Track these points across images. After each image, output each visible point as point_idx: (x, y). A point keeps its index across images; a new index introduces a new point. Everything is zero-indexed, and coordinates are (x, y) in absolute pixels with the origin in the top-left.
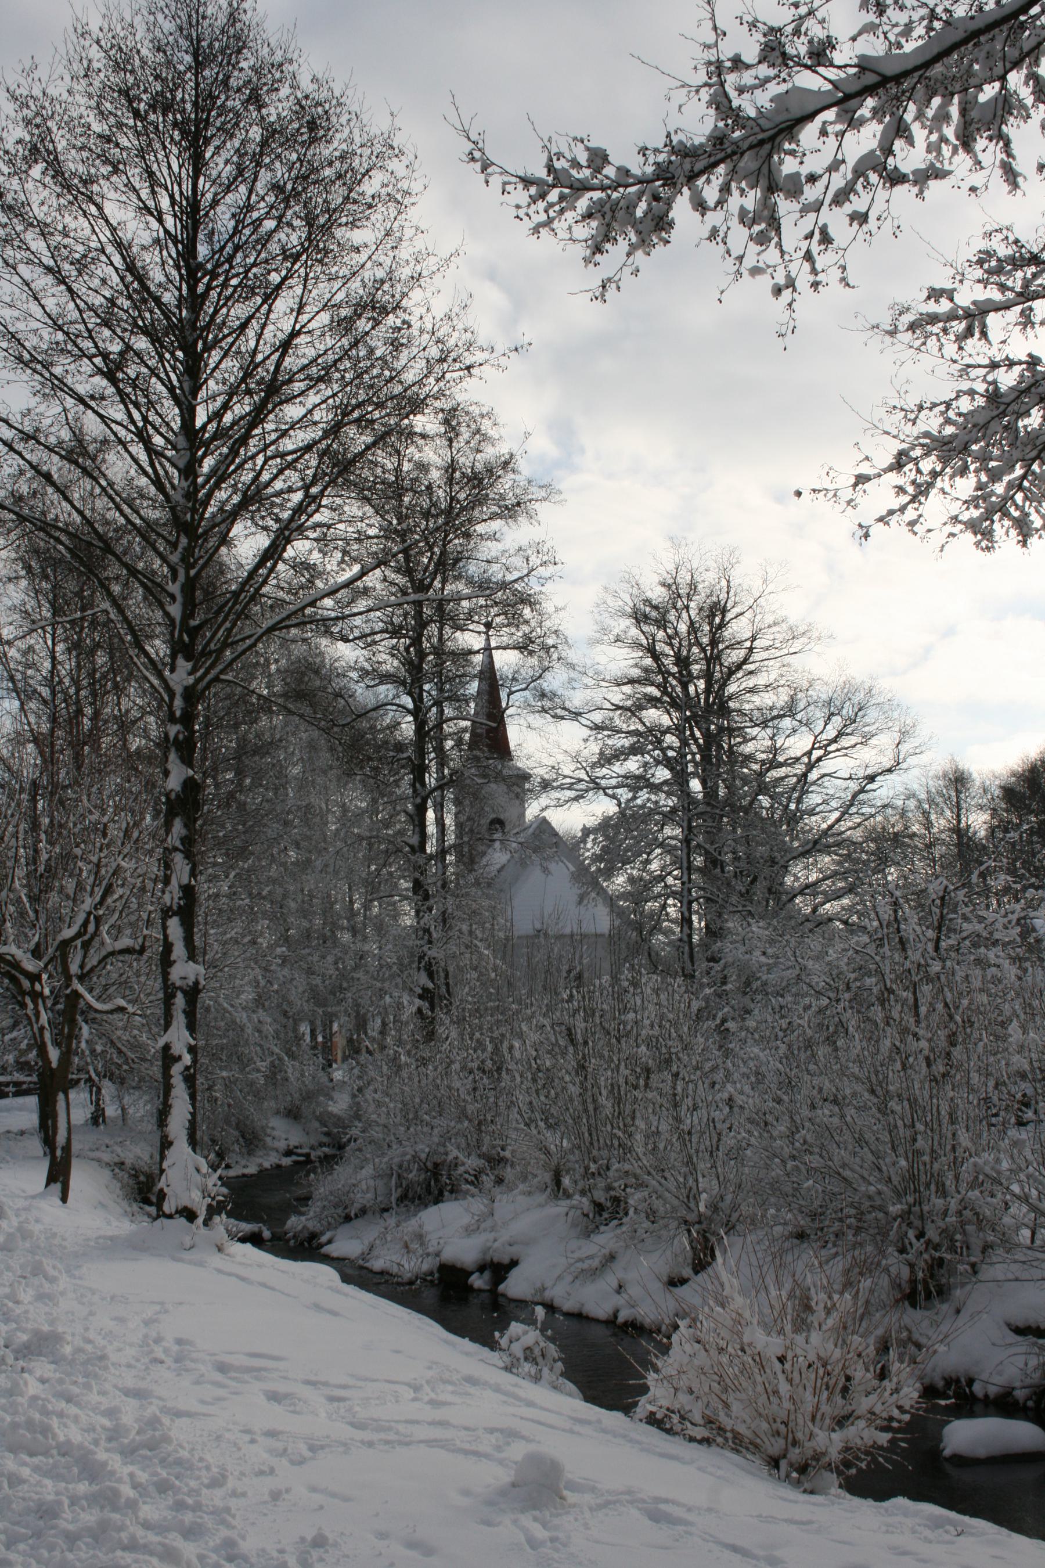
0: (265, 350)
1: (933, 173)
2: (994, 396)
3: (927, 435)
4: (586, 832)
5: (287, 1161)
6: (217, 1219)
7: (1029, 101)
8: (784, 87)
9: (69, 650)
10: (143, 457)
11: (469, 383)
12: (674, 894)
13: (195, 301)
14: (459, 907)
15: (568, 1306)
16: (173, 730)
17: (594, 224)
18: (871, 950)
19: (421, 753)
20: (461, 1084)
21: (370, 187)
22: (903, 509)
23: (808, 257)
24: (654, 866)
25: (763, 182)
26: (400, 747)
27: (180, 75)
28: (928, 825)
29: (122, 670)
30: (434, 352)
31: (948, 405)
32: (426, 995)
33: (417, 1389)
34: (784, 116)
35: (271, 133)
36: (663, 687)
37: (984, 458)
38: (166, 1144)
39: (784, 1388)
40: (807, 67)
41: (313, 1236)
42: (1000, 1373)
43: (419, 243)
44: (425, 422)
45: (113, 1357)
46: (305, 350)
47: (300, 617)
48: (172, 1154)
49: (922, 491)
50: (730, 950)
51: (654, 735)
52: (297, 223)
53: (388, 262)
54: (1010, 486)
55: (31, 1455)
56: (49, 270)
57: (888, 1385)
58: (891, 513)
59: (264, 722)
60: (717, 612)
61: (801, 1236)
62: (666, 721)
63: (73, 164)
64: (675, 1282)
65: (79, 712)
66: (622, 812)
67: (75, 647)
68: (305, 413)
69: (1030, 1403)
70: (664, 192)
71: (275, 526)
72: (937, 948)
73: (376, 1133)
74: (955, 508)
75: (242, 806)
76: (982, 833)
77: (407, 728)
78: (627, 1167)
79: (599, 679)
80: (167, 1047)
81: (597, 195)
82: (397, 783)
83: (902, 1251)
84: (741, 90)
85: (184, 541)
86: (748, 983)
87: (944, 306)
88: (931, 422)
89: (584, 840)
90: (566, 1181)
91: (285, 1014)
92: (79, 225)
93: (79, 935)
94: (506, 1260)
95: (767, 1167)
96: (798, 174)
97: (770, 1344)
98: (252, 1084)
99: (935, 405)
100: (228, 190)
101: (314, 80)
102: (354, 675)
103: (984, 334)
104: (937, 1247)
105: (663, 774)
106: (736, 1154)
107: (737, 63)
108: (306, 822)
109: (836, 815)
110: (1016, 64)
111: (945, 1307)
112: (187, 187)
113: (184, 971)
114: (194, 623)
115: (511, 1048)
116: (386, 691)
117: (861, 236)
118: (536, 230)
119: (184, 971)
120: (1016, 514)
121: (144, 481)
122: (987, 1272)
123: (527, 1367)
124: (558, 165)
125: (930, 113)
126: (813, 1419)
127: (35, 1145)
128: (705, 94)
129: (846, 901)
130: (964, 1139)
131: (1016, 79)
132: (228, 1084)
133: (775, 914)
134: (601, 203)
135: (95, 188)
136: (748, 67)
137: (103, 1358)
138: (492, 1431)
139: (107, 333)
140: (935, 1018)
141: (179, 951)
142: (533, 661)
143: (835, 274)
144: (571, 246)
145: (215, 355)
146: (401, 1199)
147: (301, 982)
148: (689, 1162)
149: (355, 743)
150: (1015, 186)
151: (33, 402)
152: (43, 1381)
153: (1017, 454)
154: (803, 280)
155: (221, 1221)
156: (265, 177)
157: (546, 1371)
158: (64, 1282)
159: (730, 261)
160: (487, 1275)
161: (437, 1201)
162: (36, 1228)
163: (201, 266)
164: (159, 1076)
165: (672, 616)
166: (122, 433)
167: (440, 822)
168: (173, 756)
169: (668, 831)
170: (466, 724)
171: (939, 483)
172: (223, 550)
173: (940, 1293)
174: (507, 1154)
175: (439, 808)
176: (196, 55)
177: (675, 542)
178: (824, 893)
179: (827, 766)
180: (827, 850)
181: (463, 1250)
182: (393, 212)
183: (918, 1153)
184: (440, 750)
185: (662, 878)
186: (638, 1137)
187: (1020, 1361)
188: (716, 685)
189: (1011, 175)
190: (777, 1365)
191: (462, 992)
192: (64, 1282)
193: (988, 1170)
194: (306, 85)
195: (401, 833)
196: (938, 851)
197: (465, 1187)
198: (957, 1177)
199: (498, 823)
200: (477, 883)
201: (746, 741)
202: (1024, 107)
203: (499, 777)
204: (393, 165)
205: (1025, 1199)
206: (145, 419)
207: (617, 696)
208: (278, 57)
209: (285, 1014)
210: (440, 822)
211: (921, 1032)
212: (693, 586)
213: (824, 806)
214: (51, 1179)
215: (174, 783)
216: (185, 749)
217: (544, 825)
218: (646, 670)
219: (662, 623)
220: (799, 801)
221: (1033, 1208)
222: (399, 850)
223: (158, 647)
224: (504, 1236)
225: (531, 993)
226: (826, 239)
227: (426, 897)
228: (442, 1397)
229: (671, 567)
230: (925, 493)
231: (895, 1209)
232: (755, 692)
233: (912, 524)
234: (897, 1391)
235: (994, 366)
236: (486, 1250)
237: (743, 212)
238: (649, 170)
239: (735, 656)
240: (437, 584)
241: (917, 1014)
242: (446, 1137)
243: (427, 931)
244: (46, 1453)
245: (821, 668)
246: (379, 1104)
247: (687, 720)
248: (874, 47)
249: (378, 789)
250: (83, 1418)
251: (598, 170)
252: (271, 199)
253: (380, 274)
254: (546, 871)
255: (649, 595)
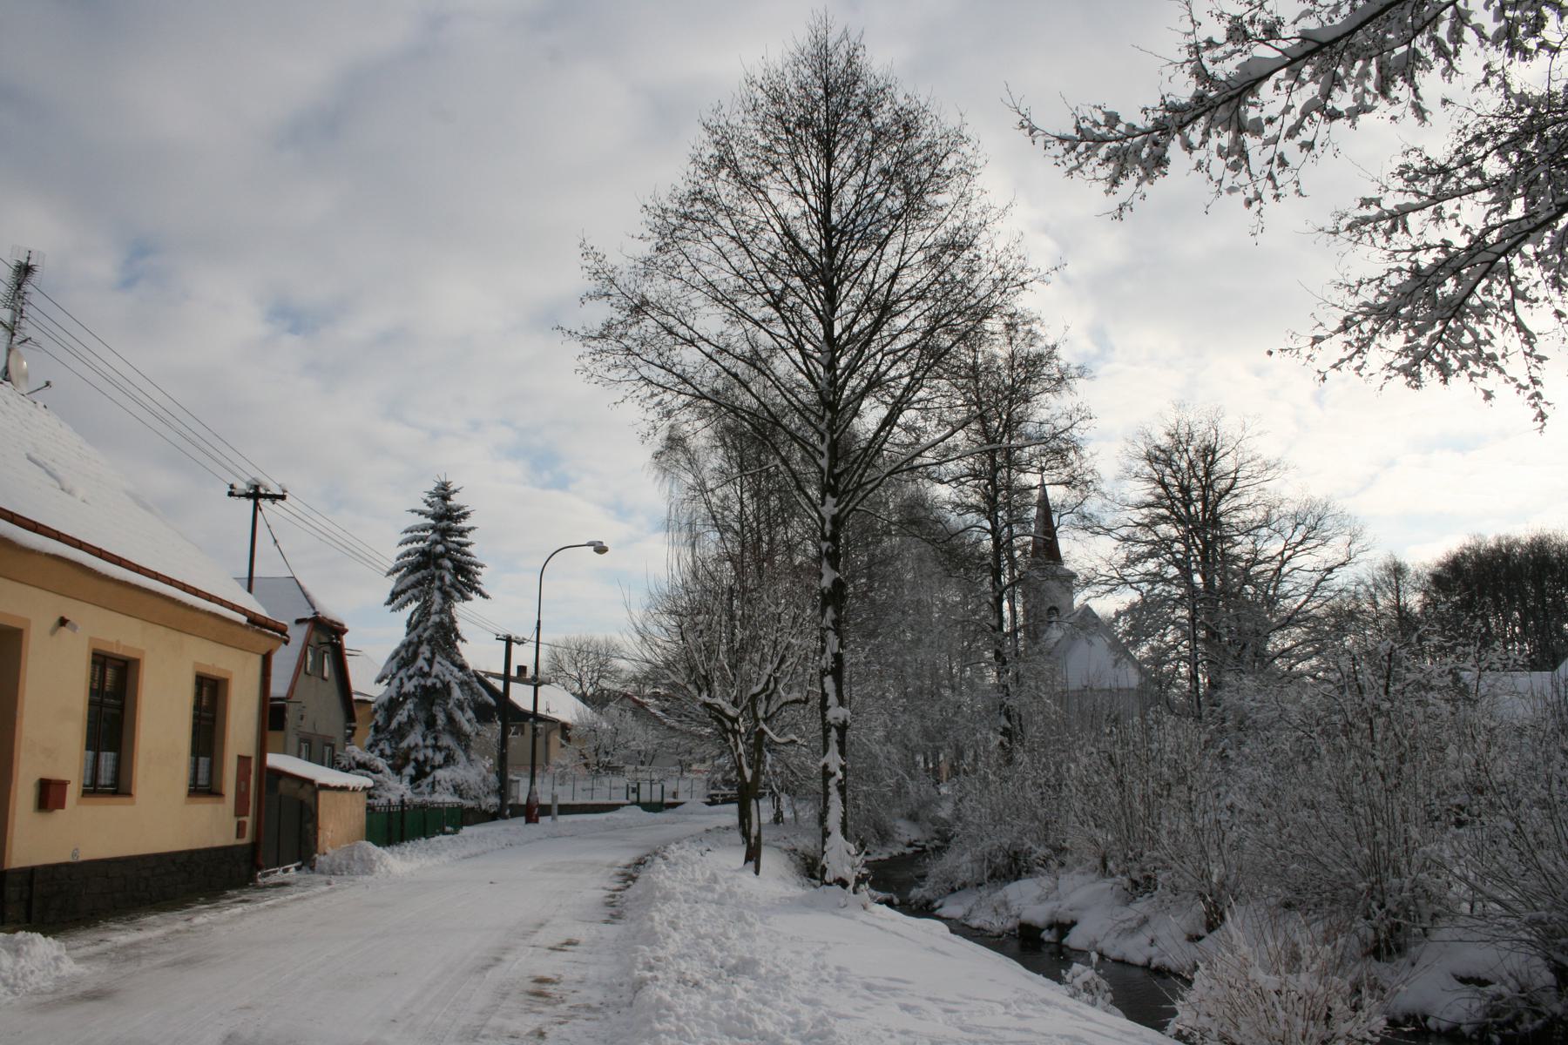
0: (879, 281)
1: (1361, 109)
2: (1416, 272)
3: (1365, 304)
4: (1118, 614)
5: (909, 851)
6: (862, 887)
7: (1431, 57)
8: (1245, 58)
9: (752, 497)
10: (799, 358)
11: (1024, 295)
12: (1183, 659)
13: (831, 252)
14: (1028, 669)
15: (1114, 954)
16: (825, 545)
17: (1111, 166)
18: (1335, 694)
19: (998, 560)
20: (1032, 795)
21: (947, 165)
22: (1350, 358)
23: (1271, 177)
24: (1168, 638)
25: (1234, 126)
26: (982, 557)
27: (815, 102)
28: (1375, 604)
29: (788, 510)
30: (998, 274)
31: (1382, 280)
32: (1006, 732)
33: (1007, 1006)
34: (1247, 78)
35: (879, 134)
36: (1171, 508)
37: (1411, 318)
38: (826, 834)
39: (1281, 1014)
40: (1261, 41)
41: (929, 902)
42: (1449, 1012)
43: (984, 201)
44: (994, 324)
45: (794, 977)
46: (907, 280)
47: (908, 467)
48: (830, 841)
49: (1364, 344)
50: (1226, 696)
51: (1166, 543)
52: (898, 193)
53: (962, 215)
54: (1432, 339)
55: (741, 1038)
56: (733, 238)
57: (1362, 1015)
58: (1342, 361)
59: (886, 543)
60: (1209, 453)
61: (1288, 905)
62: (1174, 533)
63: (748, 167)
64: (1194, 938)
65: (760, 539)
66: (1144, 600)
67: (756, 494)
68: (909, 322)
69: (1475, 1037)
70: (1162, 140)
71: (891, 401)
72: (1387, 692)
73: (973, 830)
74: (1390, 358)
75: (873, 601)
76: (1417, 609)
77: (988, 543)
78: (1156, 854)
79: (1125, 505)
80: (825, 767)
81: (1114, 144)
82: (981, 583)
83: (1368, 917)
84: (1214, 61)
85: (828, 415)
86: (1241, 722)
87: (1374, 211)
88: (1369, 294)
89: (1116, 620)
90: (1111, 865)
91: (906, 747)
92: (753, 207)
93: (763, 690)
94: (1068, 921)
95: (1262, 855)
96: (1259, 119)
97: (1270, 982)
98: (884, 796)
99: (1371, 281)
100: (851, 175)
101: (907, 96)
102: (949, 507)
103: (1405, 229)
104: (1395, 915)
105: (1173, 571)
106: (1237, 846)
107: (1210, 44)
108: (918, 612)
109: (1304, 598)
110: (1420, 31)
111: (1403, 960)
112: (823, 175)
113: (836, 713)
114: (837, 471)
115: (1069, 769)
116: (971, 517)
117: (1309, 159)
118: (1070, 173)
119: (836, 713)
120: (1438, 359)
121: (800, 376)
122: (1436, 935)
123: (1085, 996)
124: (1083, 126)
125: (1354, 73)
126: (1304, 1038)
127: (737, 836)
128: (1188, 68)
129: (1314, 662)
130: (1414, 832)
131: (1419, 42)
132: (867, 796)
133: (1261, 671)
134: (1116, 150)
135: (762, 182)
136: (1218, 45)
137: (786, 977)
138: (1063, 1037)
139: (772, 277)
140: (1387, 745)
141: (832, 699)
142: (1076, 492)
143: (1292, 187)
144: (1095, 184)
145: (847, 285)
146: (991, 877)
147: (916, 725)
148: (1202, 851)
149: (950, 552)
150: (1424, 119)
151: (724, 327)
152: (747, 991)
153: (1437, 313)
154: (1268, 194)
155: (864, 887)
156: (875, 165)
157: (1099, 999)
158: (758, 926)
159: (1213, 184)
160: (1054, 931)
161: (1016, 879)
162: (739, 891)
163: (834, 228)
164: (820, 790)
165: (1176, 457)
166: (784, 343)
167: (1012, 610)
168: (825, 563)
169: (1179, 612)
170: (1029, 539)
171: (1377, 339)
172: (856, 420)
173: (1399, 950)
174: (1067, 845)
175: (1012, 599)
176: (826, 89)
177: (1180, 406)
178: (1297, 656)
179: (1296, 562)
180: (1297, 624)
181: (1037, 914)
182: (964, 181)
183: (1378, 844)
184: (1011, 558)
185: (1175, 647)
186: (1164, 832)
187: (1465, 1004)
188: (1210, 506)
189: (1420, 112)
190: (1275, 997)
191: (1032, 730)
192: (758, 926)
193: (1434, 857)
194: (901, 101)
195: (985, 617)
196: (1383, 623)
197: (1037, 868)
198: (1409, 863)
199: (1054, 610)
200: (1041, 652)
201: (1235, 545)
202: (1428, 62)
203: (1054, 576)
204: (964, 148)
205: (1465, 879)
206: (800, 333)
207: (1138, 516)
208: (881, 85)
209: (906, 747)
210: (1012, 610)
211: (1377, 754)
212: (1191, 436)
213: (1294, 592)
214: (748, 859)
215: (826, 582)
216: (833, 558)
217: (1087, 610)
218: (1159, 497)
219: (1169, 463)
220: (1275, 588)
221: (1472, 887)
222: (984, 630)
223: (813, 492)
224: (1066, 904)
225: (1082, 730)
226: (1283, 163)
227: (1004, 663)
228: (1025, 1013)
229: (1174, 422)
230: (1368, 345)
231: (1362, 886)
232: (1240, 509)
233: (1358, 368)
234: (1368, 1018)
235: (1415, 250)
236: (1053, 914)
237: (1220, 149)
238: (1150, 124)
239: (1223, 484)
240: (1005, 440)
241: (1373, 740)
242: (1022, 833)
243: (1005, 687)
244: (750, 1038)
245: (1290, 490)
246: (974, 810)
247: (1190, 531)
248: (1311, 24)
249: (970, 588)
250: (775, 1016)
251: (1113, 127)
252: (880, 178)
253: (958, 223)
254: (1090, 643)
255: (1158, 442)
